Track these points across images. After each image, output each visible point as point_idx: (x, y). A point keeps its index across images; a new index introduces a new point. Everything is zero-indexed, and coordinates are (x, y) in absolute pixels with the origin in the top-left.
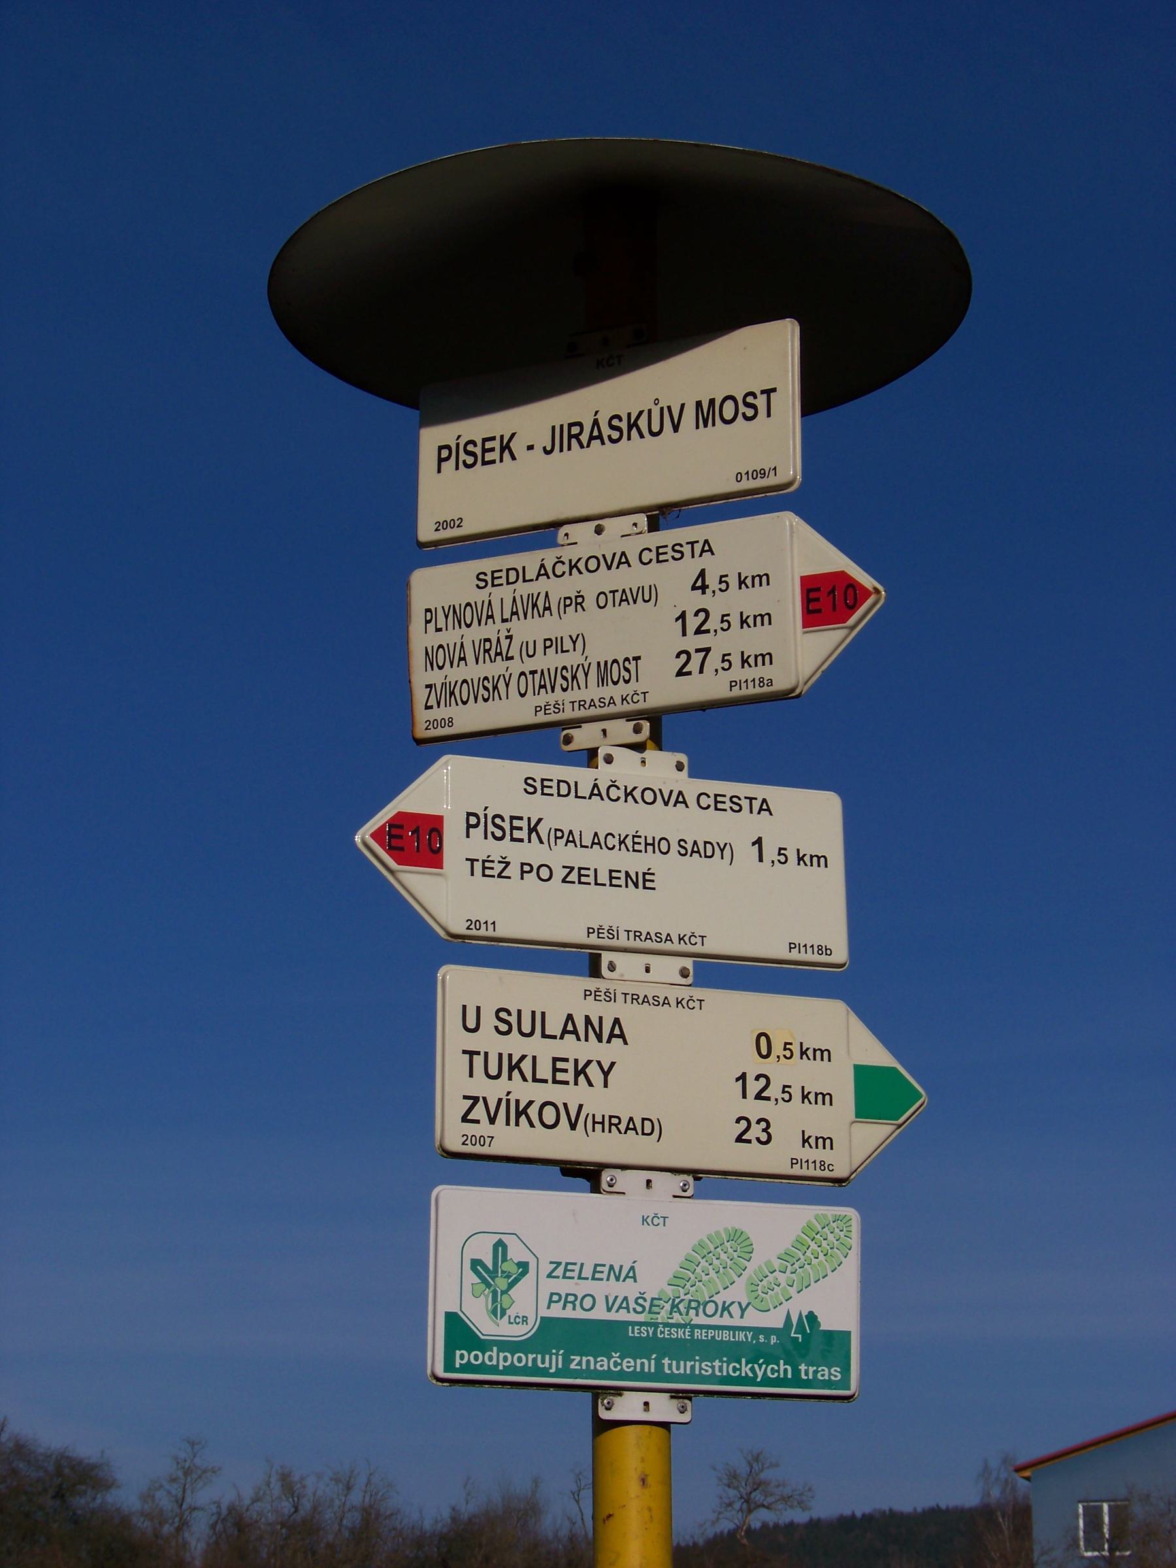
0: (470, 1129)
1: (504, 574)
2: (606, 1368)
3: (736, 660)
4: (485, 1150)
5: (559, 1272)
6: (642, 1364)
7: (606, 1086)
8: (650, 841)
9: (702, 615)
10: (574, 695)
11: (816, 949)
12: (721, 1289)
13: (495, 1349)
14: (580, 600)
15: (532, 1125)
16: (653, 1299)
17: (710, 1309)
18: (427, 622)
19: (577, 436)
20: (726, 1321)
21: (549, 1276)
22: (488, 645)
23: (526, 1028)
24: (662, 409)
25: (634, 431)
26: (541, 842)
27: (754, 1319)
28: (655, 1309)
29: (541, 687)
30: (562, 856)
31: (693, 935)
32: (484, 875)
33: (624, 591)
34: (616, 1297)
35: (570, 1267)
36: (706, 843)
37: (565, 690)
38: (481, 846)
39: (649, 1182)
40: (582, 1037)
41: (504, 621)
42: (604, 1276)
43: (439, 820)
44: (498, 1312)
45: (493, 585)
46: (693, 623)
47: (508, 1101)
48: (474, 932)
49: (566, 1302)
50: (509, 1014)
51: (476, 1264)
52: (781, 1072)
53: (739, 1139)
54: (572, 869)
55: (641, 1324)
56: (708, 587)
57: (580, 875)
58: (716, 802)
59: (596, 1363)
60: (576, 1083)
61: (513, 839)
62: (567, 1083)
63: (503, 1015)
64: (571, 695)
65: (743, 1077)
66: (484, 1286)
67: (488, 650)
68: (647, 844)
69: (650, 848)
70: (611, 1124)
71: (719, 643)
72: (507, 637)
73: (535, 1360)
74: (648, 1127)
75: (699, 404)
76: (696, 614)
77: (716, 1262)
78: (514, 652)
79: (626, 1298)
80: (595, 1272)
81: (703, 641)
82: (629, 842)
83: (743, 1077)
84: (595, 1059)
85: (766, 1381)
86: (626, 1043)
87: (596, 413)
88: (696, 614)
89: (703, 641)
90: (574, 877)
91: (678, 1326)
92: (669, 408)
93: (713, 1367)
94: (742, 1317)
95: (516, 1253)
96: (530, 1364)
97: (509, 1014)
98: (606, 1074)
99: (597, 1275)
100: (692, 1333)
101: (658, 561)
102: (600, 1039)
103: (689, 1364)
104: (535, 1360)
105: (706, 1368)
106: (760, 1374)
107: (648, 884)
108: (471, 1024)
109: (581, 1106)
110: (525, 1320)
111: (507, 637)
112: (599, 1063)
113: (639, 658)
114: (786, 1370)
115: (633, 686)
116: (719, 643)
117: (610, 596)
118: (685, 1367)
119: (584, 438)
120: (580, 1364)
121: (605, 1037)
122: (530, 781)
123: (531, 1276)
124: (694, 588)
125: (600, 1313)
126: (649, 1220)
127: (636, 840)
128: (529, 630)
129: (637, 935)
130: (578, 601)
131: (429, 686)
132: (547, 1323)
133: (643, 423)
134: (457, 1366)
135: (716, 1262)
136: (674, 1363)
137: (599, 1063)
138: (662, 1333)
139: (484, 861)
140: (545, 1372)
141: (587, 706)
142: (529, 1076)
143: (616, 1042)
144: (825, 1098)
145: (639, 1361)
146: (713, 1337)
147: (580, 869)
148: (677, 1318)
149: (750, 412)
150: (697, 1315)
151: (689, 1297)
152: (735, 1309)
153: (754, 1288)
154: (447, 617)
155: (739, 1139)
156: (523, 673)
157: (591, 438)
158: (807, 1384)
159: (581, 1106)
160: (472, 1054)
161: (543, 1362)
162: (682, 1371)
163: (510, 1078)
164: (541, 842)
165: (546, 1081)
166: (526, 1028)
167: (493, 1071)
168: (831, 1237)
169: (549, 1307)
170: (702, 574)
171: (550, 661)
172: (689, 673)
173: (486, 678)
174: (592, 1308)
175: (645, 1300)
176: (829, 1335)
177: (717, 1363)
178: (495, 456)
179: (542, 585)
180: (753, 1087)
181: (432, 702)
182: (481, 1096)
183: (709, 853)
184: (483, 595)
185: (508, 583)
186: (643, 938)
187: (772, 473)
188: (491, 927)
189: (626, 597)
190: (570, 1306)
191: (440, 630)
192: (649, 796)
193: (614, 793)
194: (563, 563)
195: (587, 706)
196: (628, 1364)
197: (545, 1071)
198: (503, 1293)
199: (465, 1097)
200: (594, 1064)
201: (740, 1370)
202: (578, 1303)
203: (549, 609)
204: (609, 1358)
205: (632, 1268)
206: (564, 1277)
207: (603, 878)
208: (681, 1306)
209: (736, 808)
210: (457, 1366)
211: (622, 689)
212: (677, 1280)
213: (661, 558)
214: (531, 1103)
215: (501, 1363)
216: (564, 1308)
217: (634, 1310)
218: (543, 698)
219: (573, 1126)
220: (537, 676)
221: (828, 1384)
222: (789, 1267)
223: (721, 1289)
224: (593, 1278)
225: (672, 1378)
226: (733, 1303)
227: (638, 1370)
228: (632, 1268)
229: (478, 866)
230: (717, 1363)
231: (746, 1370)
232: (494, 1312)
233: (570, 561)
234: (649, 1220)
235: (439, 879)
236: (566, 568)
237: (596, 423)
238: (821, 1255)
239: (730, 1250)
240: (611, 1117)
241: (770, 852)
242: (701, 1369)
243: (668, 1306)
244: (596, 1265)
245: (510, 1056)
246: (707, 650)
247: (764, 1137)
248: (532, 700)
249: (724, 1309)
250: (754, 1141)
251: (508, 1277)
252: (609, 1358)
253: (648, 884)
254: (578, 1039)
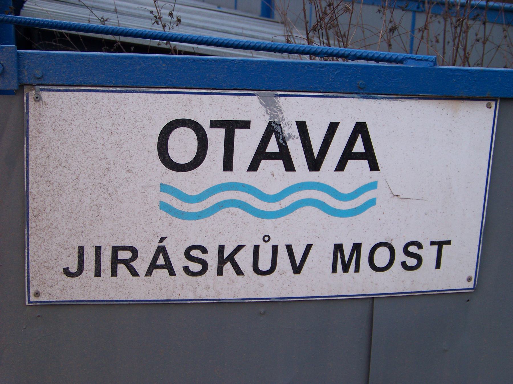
24: (275, 248)
70: (115, 261)
75: (338, 248)
87: (162, 239)
117: (216, 138)
233: (221, 249)
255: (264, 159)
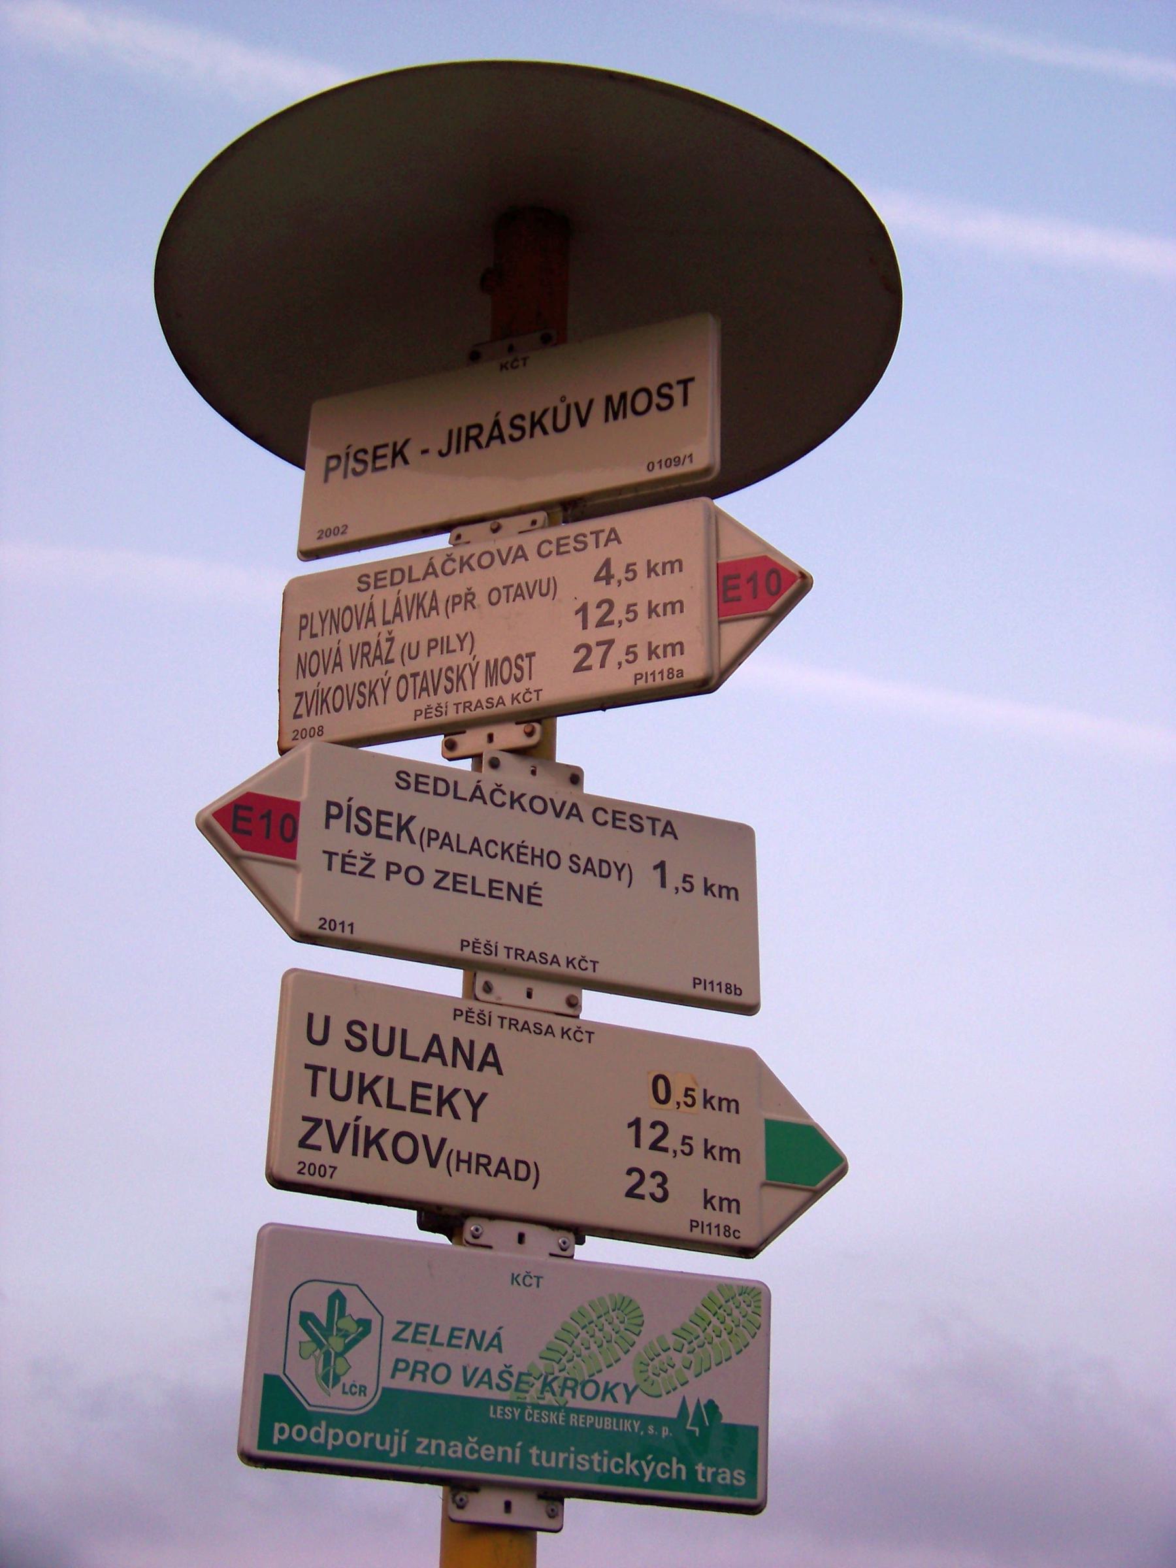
0: (308, 1156)
1: (388, 575)
2: (459, 1455)
3: (642, 652)
4: (326, 1182)
5: (408, 1334)
6: (505, 1453)
7: (475, 1119)
8: (537, 853)
9: (605, 607)
10: (461, 696)
11: (724, 987)
12: (604, 1368)
13: (323, 1424)
14: (470, 597)
15: (384, 1158)
16: (521, 1374)
17: (590, 1390)
18: (302, 628)
19: (475, 438)
20: (608, 1405)
21: (396, 1338)
22: (366, 649)
23: (383, 1045)
24: (569, 407)
25: (538, 430)
26: (412, 841)
27: (642, 1405)
28: (523, 1386)
29: (422, 690)
30: (435, 859)
31: (583, 959)
32: (343, 871)
33: (519, 586)
34: (476, 1369)
35: (421, 1329)
36: (601, 861)
37: (448, 692)
38: (340, 838)
39: (521, 1238)
40: (449, 1059)
41: (385, 623)
42: (463, 1342)
43: (296, 806)
44: (329, 1378)
45: (376, 587)
46: (594, 615)
47: (357, 1128)
48: (328, 932)
49: (415, 1371)
50: (364, 1027)
51: (306, 1318)
52: (680, 1121)
53: (630, 1193)
54: (446, 874)
55: (505, 1403)
56: (613, 577)
57: (455, 882)
58: (614, 819)
59: (448, 1447)
60: (439, 1114)
61: (379, 835)
62: (428, 1112)
63: (357, 1028)
64: (455, 697)
65: (636, 1123)
66: (314, 1346)
67: (366, 654)
68: (534, 856)
69: (537, 861)
70: (478, 1164)
71: (624, 636)
72: (387, 640)
73: (372, 1440)
74: (523, 1171)
76: (599, 606)
77: (599, 1334)
78: (395, 654)
79: (488, 1371)
80: (451, 1336)
81: (605, 633)
82: (513, 851)
83: (636, 1123)
84: (463, 1088)
85: (655, 1482)
86: (500, 1072)
87: (500, 1328)
88: (599, 606)
89: (605, 633)
90: (448, 882)
91: (550, 1408)
92: (577, 405)
93: (591, 1462)
94: (628, 1402)
95: (356, 1307)
96: (366, 1445)
97: (369, 813)
98: (475, 1106)
99: (454, 1341)
100: (567, 1417)
101: (558, 553)
102: (470, 1066)
103: (562, 1456)
104: (372, 1440)
105: (582, 1462)
106: (648, 1473)
107: (533, 899)
108: (318, 1035)
109: (443, 1141)
110: (363, 1390)
111: (387, 640)
112: (468, 1093)
113: (533, 654)
114: (679, 1470)
115: (525, 684)
116: (624, 636)
117: (504, 593)
118: (557, 1460)
119: (483, 440)
120: (428, 1447)
121: (476, 1064)
122: (403, 775)
123: (372, 1339)
124: (597, 579)
125: (455, 1387)
126: (520, 1279)
127: (522, 850)
128: (409, 631)
129: (519, 953)
130: (468, 599)
131: (299, 694)
132: (390, 1396)
133: (548, 421)
134: (275, 1441)
135: (599, 1334)
136: (544, 1453)
137: (468, 1093)
138: (530, 1415)
139: (344, 856)
140: (384, 1456)
141: (473, 708)
142: (383, 1099)
143: (490, 1071)
144: (732, 1154)
145: (500, 1449)
146: (592, 1425)
147: (455, 875)
148: (549, 1399)
149: (664, 403)
150: (574, 1396)
151: (564, 1374)
152: (620, 1393)
153: (643, 1368)
154: (323, 621)
155: (630, 1193)
156: (403, 677)
157: (491, 438)
158: (706, 1488)
159: (443, 1141)
160: (316, 1069)
161: (383, 1443)
162: (553, 1464)
163: (360, 1101)
164: (412, 841)
165: (403, 1108)
166: (383, 1045)
167: (341, 1090)
168: (736, 1312)
169: (393, 1376)
170: (607, 564)
171: (436, 661)
172: (589, 668)
173: (363, 684)
174: (446, 1381)
175: (511, 1374)
176: (732, 1429)
177: (596, 1457)
178: (387, 462)
179: (431, 584)
180: (648, 1136)
181: (302, 710)
182: (324, 1117)
183: (605, 872)
184: (365, 598)
185: (392, 584)
186: (525, 956)
187: (687, 460)
188: (347, 929)
189: (522, 592)
190: (419, 1376)
191: (316, 636)
192: (538, 804)
193: (499, 798)
194: (454, 561)
195: (473, 708)
196: (487, 1452)
197: (402, 1096)
198: (338, 1355)
199: (305, 1119)
200: (462, 1094)
201: (624, 1466)
202: (429, 1373)
203: (436, 608)
204: (465, 1442)
205: (497, 1335)
206: (414, 1340)
207: (482, 887)
208: (555, 1385)
209: (637, 827)
210: (275, 1441)
211: (514, 687)
212: (551, 1353)
213: (562, 549)
214: (383, 1132)
215: (331, 1441)
216: (412, 1377)
217: (498, 1386)
218: (425, 701)
219: (433, 1163)
220: (419, 679)
221: (730, 1489)
222: (686, 1346)
223: (604, 1368)
224: (449, 1345)
225: (541, 1472)
226: (617, 1384)
227: (500, 1459)
228: (497, 1335)
229: (337, 861)
230: (596, 1457)
231: (631, 1467)
232: (325, 1378)
234: (520, 1279)
235: (291, 870)
236: (457, 565)
237: (497, 424)
238: (724, 1334)
239: (616, 1321)
240: (479, 1156)
241: (674, 879)
242: (576, 1462)
243: (538, 1384)
244: (453, 1329)
245: (362, 1076)
246: (610, 643)
247: (659, 1193)
248: (411, 704)
249: (606, 1391)
250: (648, 1197)
251: (346, 1336)
252: (464, 1444)
253: (533, 899)
254: (445, 1063)
255: (671, 1419)
